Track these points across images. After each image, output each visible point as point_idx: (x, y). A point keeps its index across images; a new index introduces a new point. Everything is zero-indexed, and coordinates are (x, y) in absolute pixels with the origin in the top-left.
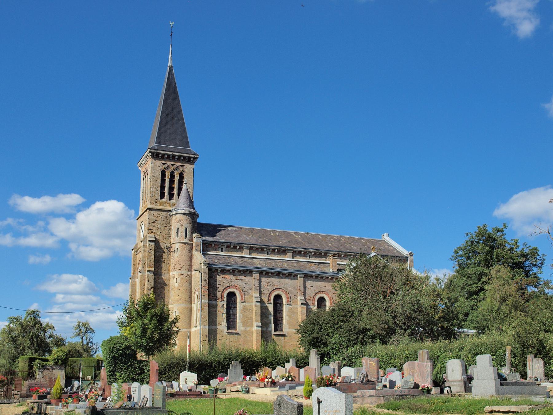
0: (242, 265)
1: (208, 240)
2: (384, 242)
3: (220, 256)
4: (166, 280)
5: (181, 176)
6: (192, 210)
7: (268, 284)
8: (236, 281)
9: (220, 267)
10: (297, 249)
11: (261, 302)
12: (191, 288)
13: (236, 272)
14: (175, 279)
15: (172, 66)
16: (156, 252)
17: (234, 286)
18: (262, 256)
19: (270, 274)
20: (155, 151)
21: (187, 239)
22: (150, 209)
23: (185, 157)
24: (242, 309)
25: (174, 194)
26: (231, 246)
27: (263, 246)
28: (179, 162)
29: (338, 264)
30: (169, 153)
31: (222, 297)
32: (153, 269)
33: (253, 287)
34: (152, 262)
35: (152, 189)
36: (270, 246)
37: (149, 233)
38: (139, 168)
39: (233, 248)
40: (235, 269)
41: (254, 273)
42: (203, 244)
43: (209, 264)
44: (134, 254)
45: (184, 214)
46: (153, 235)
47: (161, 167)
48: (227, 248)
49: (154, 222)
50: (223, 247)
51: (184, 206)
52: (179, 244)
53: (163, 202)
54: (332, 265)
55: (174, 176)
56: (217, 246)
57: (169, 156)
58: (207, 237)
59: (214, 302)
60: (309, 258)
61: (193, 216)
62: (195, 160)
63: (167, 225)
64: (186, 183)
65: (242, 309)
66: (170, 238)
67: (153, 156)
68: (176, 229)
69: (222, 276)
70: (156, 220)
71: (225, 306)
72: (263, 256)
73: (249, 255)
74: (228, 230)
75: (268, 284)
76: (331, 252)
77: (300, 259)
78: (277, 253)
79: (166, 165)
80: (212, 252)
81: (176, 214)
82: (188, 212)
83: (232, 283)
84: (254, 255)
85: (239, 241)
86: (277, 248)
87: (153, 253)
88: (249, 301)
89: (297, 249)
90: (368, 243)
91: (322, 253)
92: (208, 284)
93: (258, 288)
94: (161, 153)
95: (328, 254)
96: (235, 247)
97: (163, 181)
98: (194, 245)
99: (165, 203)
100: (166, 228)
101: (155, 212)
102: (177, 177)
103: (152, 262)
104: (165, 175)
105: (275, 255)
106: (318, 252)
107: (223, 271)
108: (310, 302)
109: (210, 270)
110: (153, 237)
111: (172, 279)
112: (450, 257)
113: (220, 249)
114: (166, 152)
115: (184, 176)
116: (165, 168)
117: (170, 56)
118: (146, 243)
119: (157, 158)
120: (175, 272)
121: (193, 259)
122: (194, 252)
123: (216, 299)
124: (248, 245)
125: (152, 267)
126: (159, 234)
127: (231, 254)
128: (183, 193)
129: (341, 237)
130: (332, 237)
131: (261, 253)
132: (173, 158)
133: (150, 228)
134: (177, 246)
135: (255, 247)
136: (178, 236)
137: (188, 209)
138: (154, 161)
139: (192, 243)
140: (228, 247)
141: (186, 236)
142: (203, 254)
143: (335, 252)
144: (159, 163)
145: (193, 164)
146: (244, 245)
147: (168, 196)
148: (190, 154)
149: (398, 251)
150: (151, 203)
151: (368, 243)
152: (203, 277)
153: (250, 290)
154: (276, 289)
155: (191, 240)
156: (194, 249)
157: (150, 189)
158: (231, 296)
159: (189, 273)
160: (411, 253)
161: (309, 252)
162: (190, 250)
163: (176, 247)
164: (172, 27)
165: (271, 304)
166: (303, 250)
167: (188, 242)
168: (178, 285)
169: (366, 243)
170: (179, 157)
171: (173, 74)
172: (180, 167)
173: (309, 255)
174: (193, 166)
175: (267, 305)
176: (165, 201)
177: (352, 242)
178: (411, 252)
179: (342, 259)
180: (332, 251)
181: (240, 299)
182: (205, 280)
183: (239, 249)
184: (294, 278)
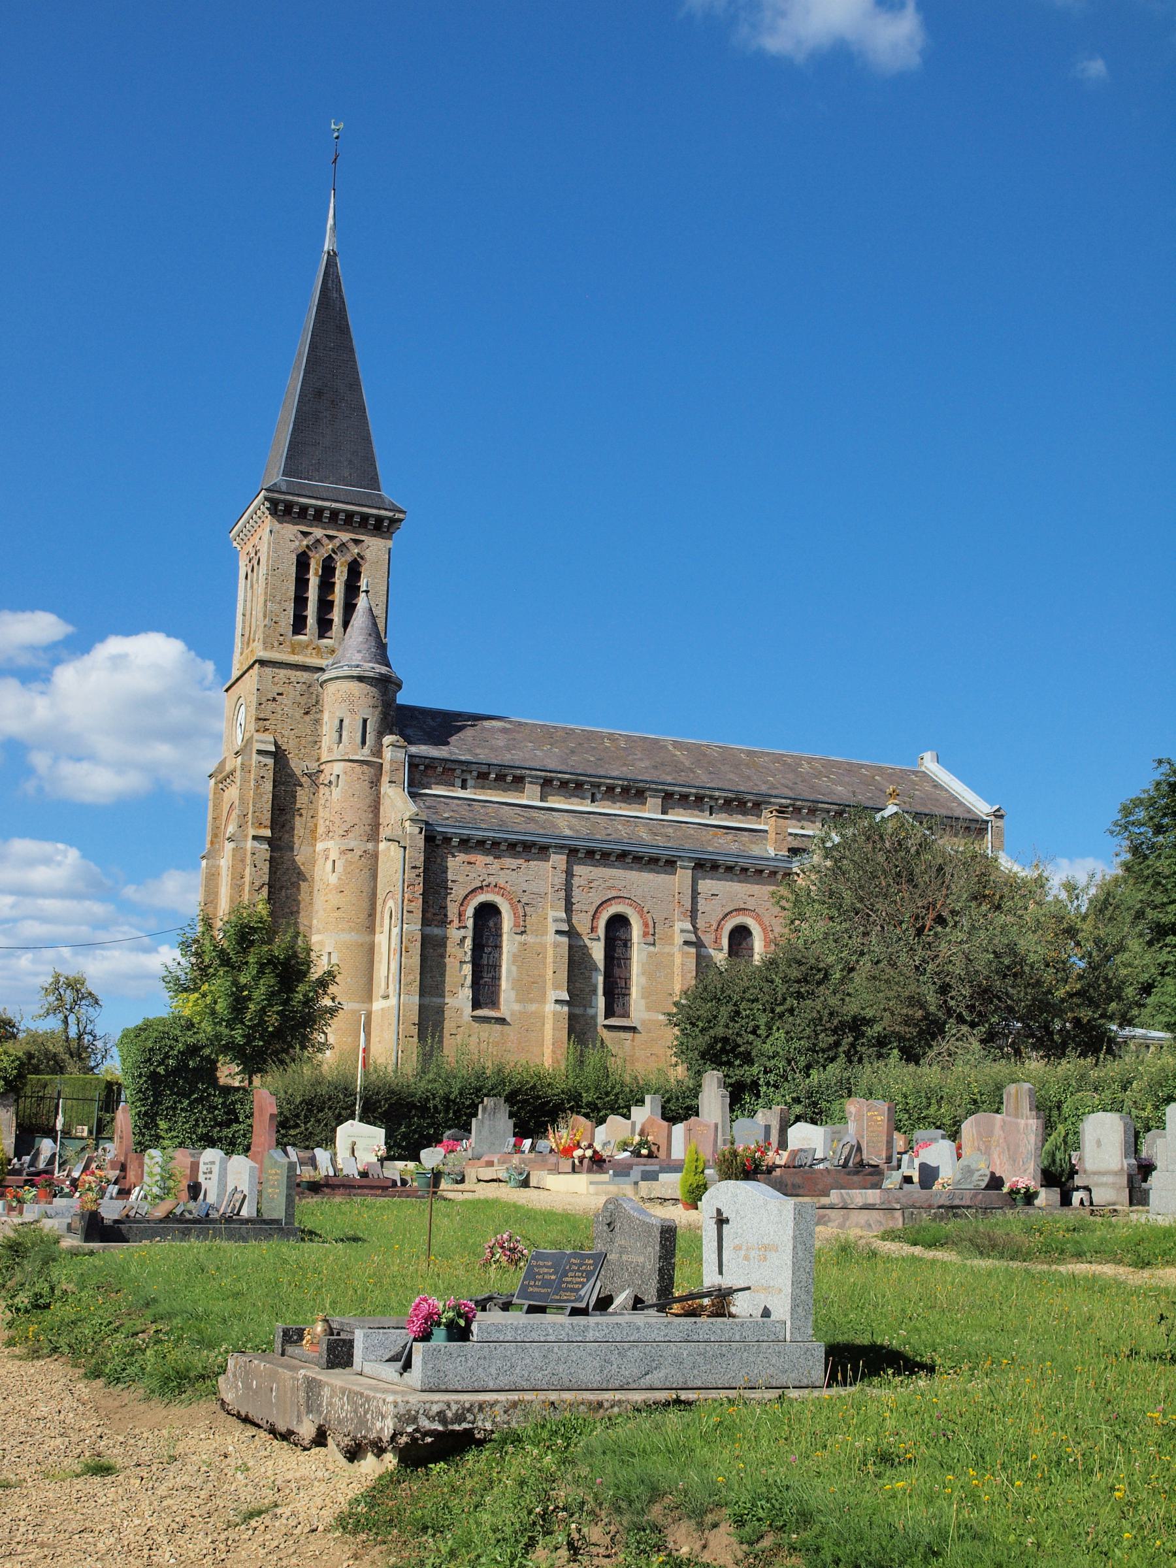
0: (521, 828)
1: (424, 754)
4: (303, 864)
5: (354, 571)
6: (384, 670)
7: (592, 885)
8: (501, 872)
10: (676, 789)
11: (571, 933)
12: (375, 887)
13: (503, 847)
14: (329, 864)
15: (335, 253)
16: (276, 784)
17: (496, 886)
18: (578, 805)
20: (282, 497)
21: (366, 751)
22: (262, 663)
23: (365, 518)
24: (515, 950)
28: (345, 531)
29: (790, 834)
30: (319, 503)
32: (268, 833)
34: (265, 812)
35: (269, 604)
36: (600, 777)
37: (257, 731)
40: (499, 840)
41: (554, 853)
43: (427, 823)
44: (215, 789)
45: (360, 679)
47: (297, 543)
49: (274, 700)
50: (469, 777)
51: (358, 656)
52: (342, 764)
53: (300, 643)
55: (335, 569)
56: (450, 771)
57: (319, 511)
59: (436, 931)
60: (711, 814)
61: (386, 685)
62: (396, 525)
63: (311, 708)
66: (317, 747)
67: (273, 511)
68: (337, 722)
69: (462, 857)
70: (278, 694)
71: (468, 943)
72: (582, 804)
73: (542, 800)
75: (592, 885)
76: (773, 800)
77: (683, 816)
78: (620, 798)
79: (310, 537)
80: (436, 789)
81: (337, 678)
82: (371, 674)
83: (492, 880)
86: (620, 782)
87: (268, 786)
89: (676, 789)
90: (877, 778)
91: (745, 803)
93: (563, 894)
94: (297, 503)
95: (763, 806)
96: (500, 778)
97: (301, 583)
99: (307, 646)
100: (307, 718)
101: (277, 671)
102: (342, 572)
103: (265, 812)
107: (466, 844)
109: (430, 839)
111: (320, 862)
113: (458, 782)
114: (313, 502)
115: (363, 569)
116: (307, 546)
117: (330, 222)
118: (251, 759)
119: (287, 518)
120: (330, 844)
122: (386, 788)
123: (444, 922)
126: (286, 733)
127: (491, 796)
128: (359, 619)
129: (801, 758)
133: (262, 716)
134: (338, 768)
135: (559, 779)
136: (340, 741)
137: (371, 665)
138: (277, 526)
139: (380, 761)
140: (483, 776)
141: (364, 742)
142: (409, 793)
143: (783, 801)
144: (290, 530)
145: (390, 538)
146: (528, 772)
147: (316, 626)
148: (379, 508)
149: (961, 804)
150: (267, 645)
151: (877, 778)
153: (539, 900)
154: (614, 898)
155: (378, 752)
156: (385, 779)
157: (266, 606)
158: (487, 914)
159: (370, 846)
160: (998, 810)
161: (711, 797)
162: (375, 783)
163: (335, 773)
165: (599, 939)
166: (693, 791)
167: (369, 759)
169: (873, 777)
170: (350, 516)
171: (338, 277)
172: (351, 545)
173: (711, 807)
174: (390, 544)
177: (833, 773)
178: (997, 807)
179: (803, 819)
180: (776, 797)
184: (666, 868)
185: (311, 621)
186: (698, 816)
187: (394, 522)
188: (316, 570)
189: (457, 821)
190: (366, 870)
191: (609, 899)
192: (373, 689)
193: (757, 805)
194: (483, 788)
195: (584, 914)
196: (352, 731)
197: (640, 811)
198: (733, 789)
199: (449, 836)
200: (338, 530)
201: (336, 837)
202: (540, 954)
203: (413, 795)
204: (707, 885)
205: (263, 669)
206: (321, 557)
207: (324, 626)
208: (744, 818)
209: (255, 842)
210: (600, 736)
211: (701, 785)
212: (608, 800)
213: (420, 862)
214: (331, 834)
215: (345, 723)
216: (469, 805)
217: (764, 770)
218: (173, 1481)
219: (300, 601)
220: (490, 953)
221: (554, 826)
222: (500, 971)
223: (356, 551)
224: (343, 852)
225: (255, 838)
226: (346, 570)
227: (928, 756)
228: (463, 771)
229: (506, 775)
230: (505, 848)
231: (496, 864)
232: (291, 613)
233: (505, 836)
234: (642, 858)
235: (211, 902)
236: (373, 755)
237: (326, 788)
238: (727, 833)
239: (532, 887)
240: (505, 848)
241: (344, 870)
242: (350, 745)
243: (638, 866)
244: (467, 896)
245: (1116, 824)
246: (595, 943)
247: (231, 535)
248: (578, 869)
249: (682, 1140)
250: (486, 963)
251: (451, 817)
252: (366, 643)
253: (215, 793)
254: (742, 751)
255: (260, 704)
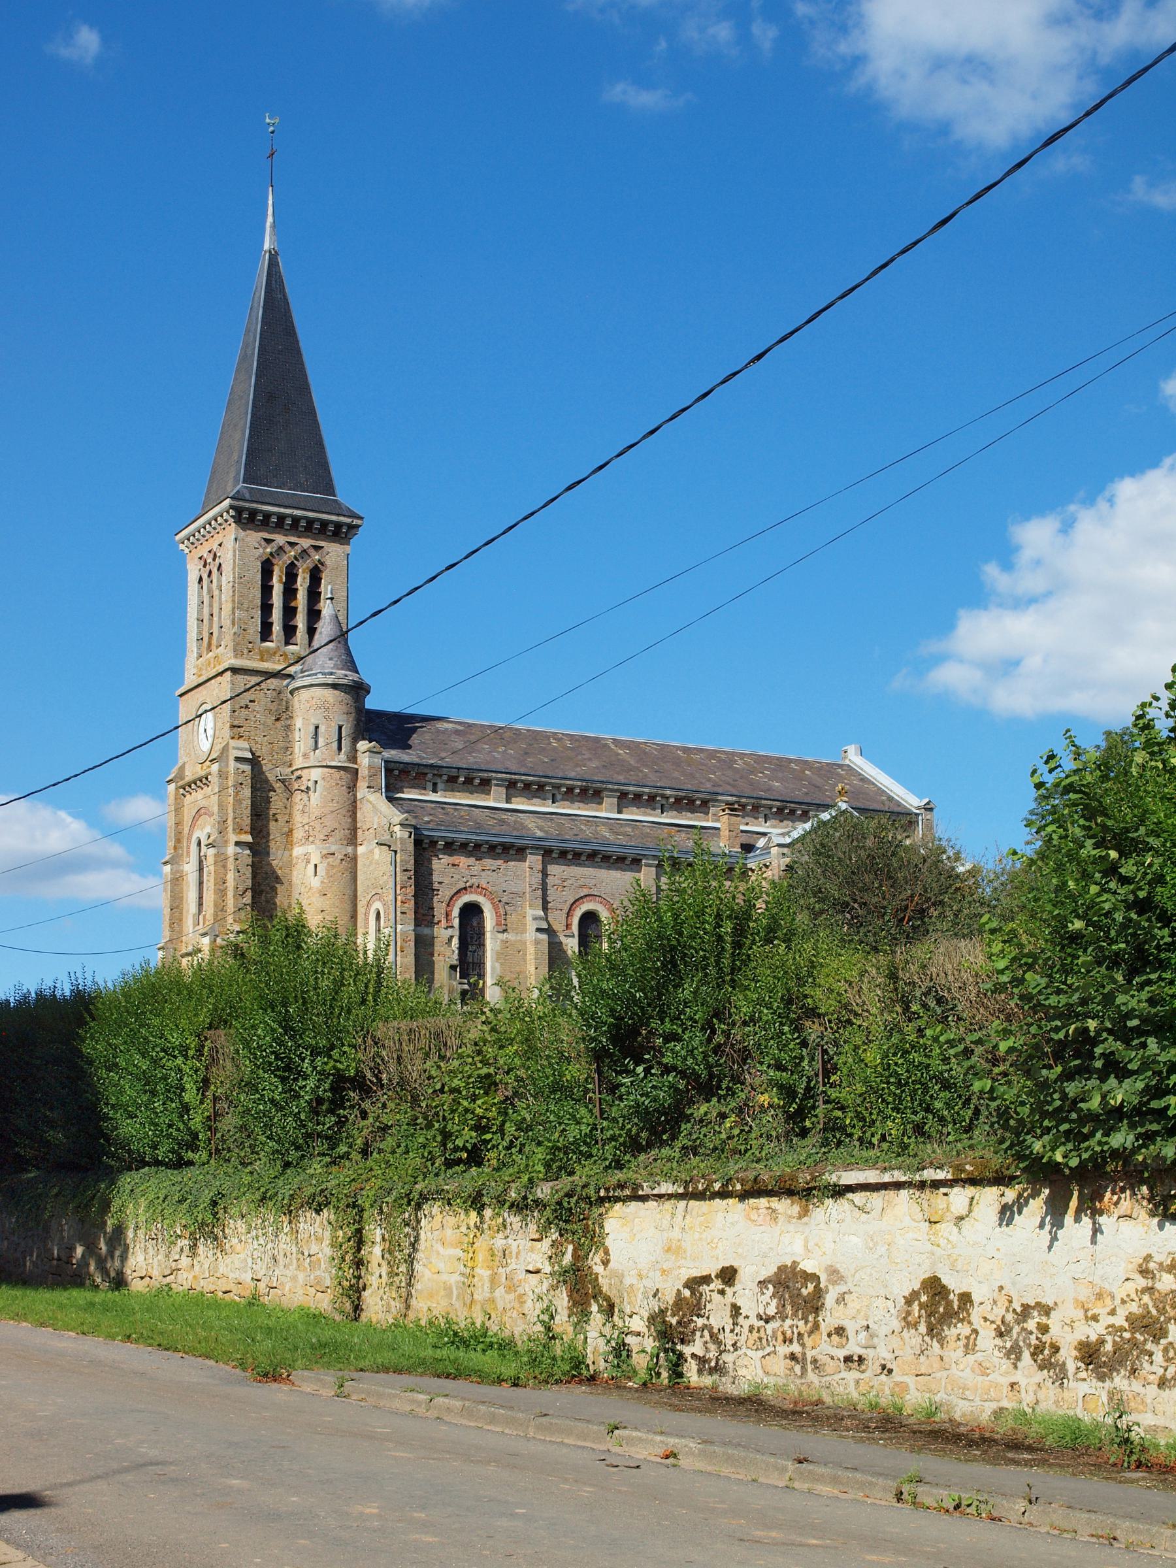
0: (496, 832)
1: (397, 759)
2: (849, 769)
3: (433, 805)
4: (280, 869)
5: (315, 576)
6: (354, 677)
7: (565, 884)
8: (483, 874)
9: (443, 835)
10: (631, 788)
11: (550, 931)
12: (356, 890)
13: (484, 848)
14: (311, 867)
15: (276, 252)
16: (254, 789)
17: (478, 887)
18: (540, 806)
19: (570, 857)
20: (247, 505)
21: (343, 756)
22: (235, 670)
23: (325, 524)
24: (498, 948)
25: (296, 627)
26: (458, 777)
27: (543, 780)
28: (307, 537)
29: (743, 831)
30: (282, 510)
31: (447, 915)
32: (248, 838)
33: (528, 889)
34: (245, 818)
35: (237, 612)
36: (561, 778)
37: (233, 738)
38: (182, 547)
39: (464, 783)
40: (480, 842)
41: (531, 854)
42: (387, 770)
43: (415, 828)
44: (176, 794)
45: (335, 686)
46: (243, 744)
47: (261, 550)
48: (447, 781)
49: (247, 707)
50: (438, 781)
51: (331, 664)
52: (320, 769)
53: (268, 650)
54: (727, 833)
55: (297, 575)
56: (417, 775)
57: (282, 518)
58: (393, 752)
59: (426, 931)
60: (662, 813)
61: (358, 690)
62: (353, 531)
63: (282, 714)
64: (332, 599)
65: (498, 948)
66: (289, 753)
67: (238, 520)
68: (312, 729)
69: (446, 859)
70: (251, 701)
71: (455, 942)
72: (544, 805)
73: (507, 802)
74: (438, 731)
75: (565, 884)
76: (720, 798)
77: (637, 814)
78: (579, 799)
79: (273, 544)
80: (409, 793)
81: (311, 686)
82: (345, 682)
83: (474, 880)
84: (518, 803)
85: (476, 763)
86: (579, 783)
87: (247, 792)
88: (516, 929)
89: (631, 788)
90: (807, 772)
91: (694, 801)
92: (412, 881)
93: (540, 892)
94: (261, 511)
95: (711, 804)
96: (469, 781)
97: (267, 590)
98: (363, 772)
99: (275, 653)
100: (278, 724)
101: (248, 678)
102: (304, 578)
103: (245, 818)
104: (272, 572)
105: (572, 802)
106: (684, 798)
107: (451, 847)
108: (558, 926)
109: (418, 843)
110: (246, 750)
111: (300, 865)
112: (1025, 814)
113: (429, 785)
114: (276, 509)
115: (323, 576)
116: (271, 554)
117: (270, 219)
118: (227, 766)
119: (250, 526)
120: (311, 848)
121: (358, 811)
122: (362, 791)
123: (431, 923)
124: (504, 776)
125: (246, 832)
126: (259, 740)
127: (460, 798)
128: (325, 629)
129: (733, 754)
130: (712, 754)
131: (537, 797)
132: (296, 526)
133: (236, 723)
134: (316, 774)
135: (522, 781)
136: (316, 748)
137: (343, 672)
138: (242, 534)
139: (356, 766)
140: (452, 780)
141: (340, 749)
142: (387, 797)
143: (729, 798)
144: (254, 537)
145: (348, 544)
146: (494, 775)
147: (282, 633)
148: (338, 515)
149: (890, 799)
150: (237, 653)
151: (807, 772)
152: (401, 861)
153: (518, 899)
154: (586, 896)
155: (353, 758)
156: (362, 785)
157: (234, 613)
158: (471, 912)
159: (350, 849)
160: (928, 803)
161: (663, 796)
162: (352, 787)
163: (313, 778)
164: (272, 132)
165: (573, 936)
166: (646, 790)
167: (346, 765)
168: (322, 882)
169: (803, 772)
170: (310, 522)
171: (280, 277)
172: (312, 552)
173: (662, 805)
174: (348, 549)
175: (563, 939)
176: (273, 648)
177: (766, 769)
178: (927, 800)
179: (748, 816)
180: (722, 794)
181: (494, 924)
182: (406, 870)
183: (480, 784)
184: (632, 866)
185: (277, 628)
186: (650, 815)
187: (352, 528)
188: (280, 577)
189: (438, 825)
190: (347, 873)
191: (582, 898)
192: (346, 696)
193: (705, 803)
194: (453, 790)
195: (559, 912)
196: (328, 734)
197: (597, 810)
198: (682, 787)
199: (435, 839)
200: (299, 537)
201: (317, 841)
202: (521, 951)
203: (390, 799)
204: (557, 871)
205: (235, 677)
206: (283, 564)
207: (289, 631)
208: (692, 815)
209: (237, 848)
210: (544, 736)
211: (652, 784)
212: (567, 800)
213: (411, 865)
214: (311, 839)
215: (322, 729)
216: (443, 808)
217: (704, 767)
218: (704, 1236)
219: (266, 608)
220: (475, 952)
221: (524, 827)
222: (484, 968)
223: (317, 557)
224: (325, 856)
225: (237, 844)
226: (308, 577)
227: (852, 750)
228: (434, 775)
229: (474, 778)
230: (486, 850)
231: (477, 866)
232: (258, 620)
233: (486, 838)
234: (610, 857)
235: (177, 907)
236: (349, 760)
237: (304, 796)
238: (679, 831)
239: (513, 887)
240: (486, 850)
241: (327, 874)
242: (327, 753)
243: (608, 864)
244: (453, 896)
245: (1032, 813)
246: (570, 939)
247: (178, 538)
248: (553, 869)
249: (18, 1292)
250: (471, 960)
251: (431, 821)
252: (336, 650)
253: (176, 799)
254: (678, 748)
255: (234, 711)
